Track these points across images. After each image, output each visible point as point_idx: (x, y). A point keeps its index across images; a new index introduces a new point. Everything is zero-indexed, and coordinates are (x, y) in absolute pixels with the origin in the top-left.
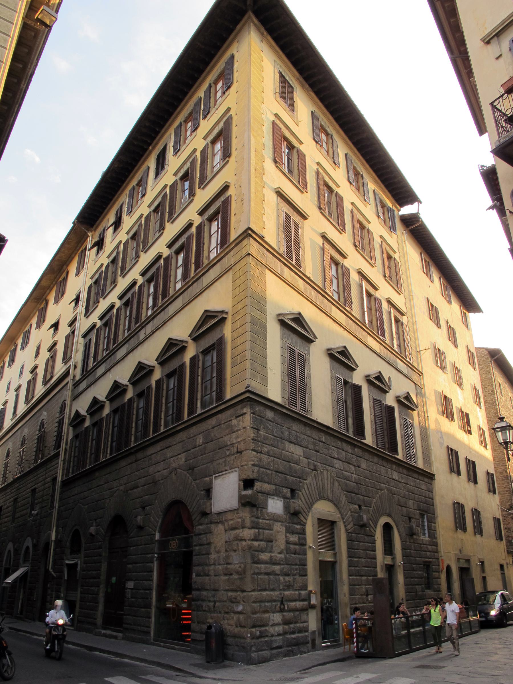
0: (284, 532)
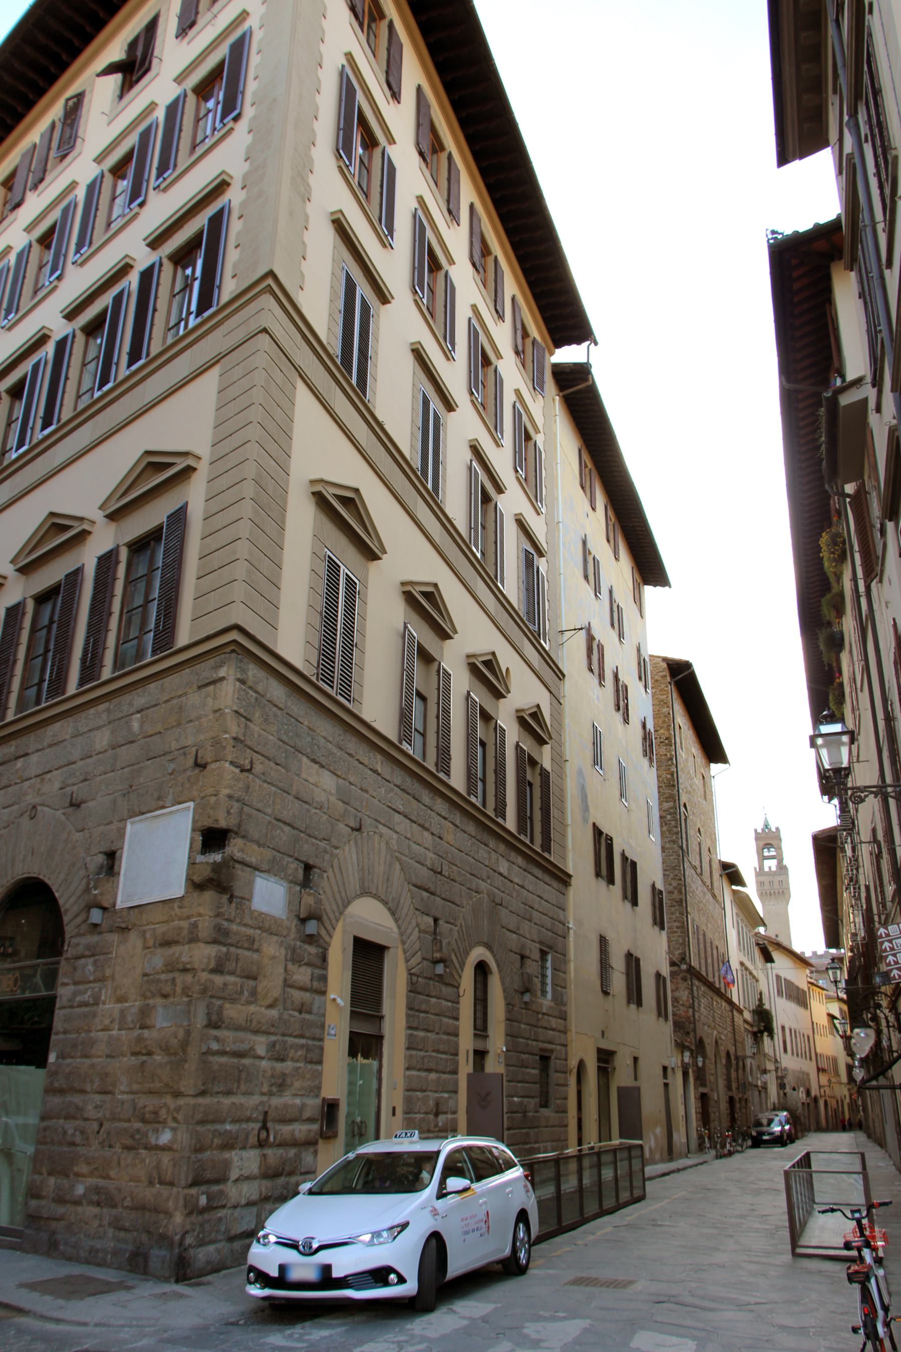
0: (283, 958)
